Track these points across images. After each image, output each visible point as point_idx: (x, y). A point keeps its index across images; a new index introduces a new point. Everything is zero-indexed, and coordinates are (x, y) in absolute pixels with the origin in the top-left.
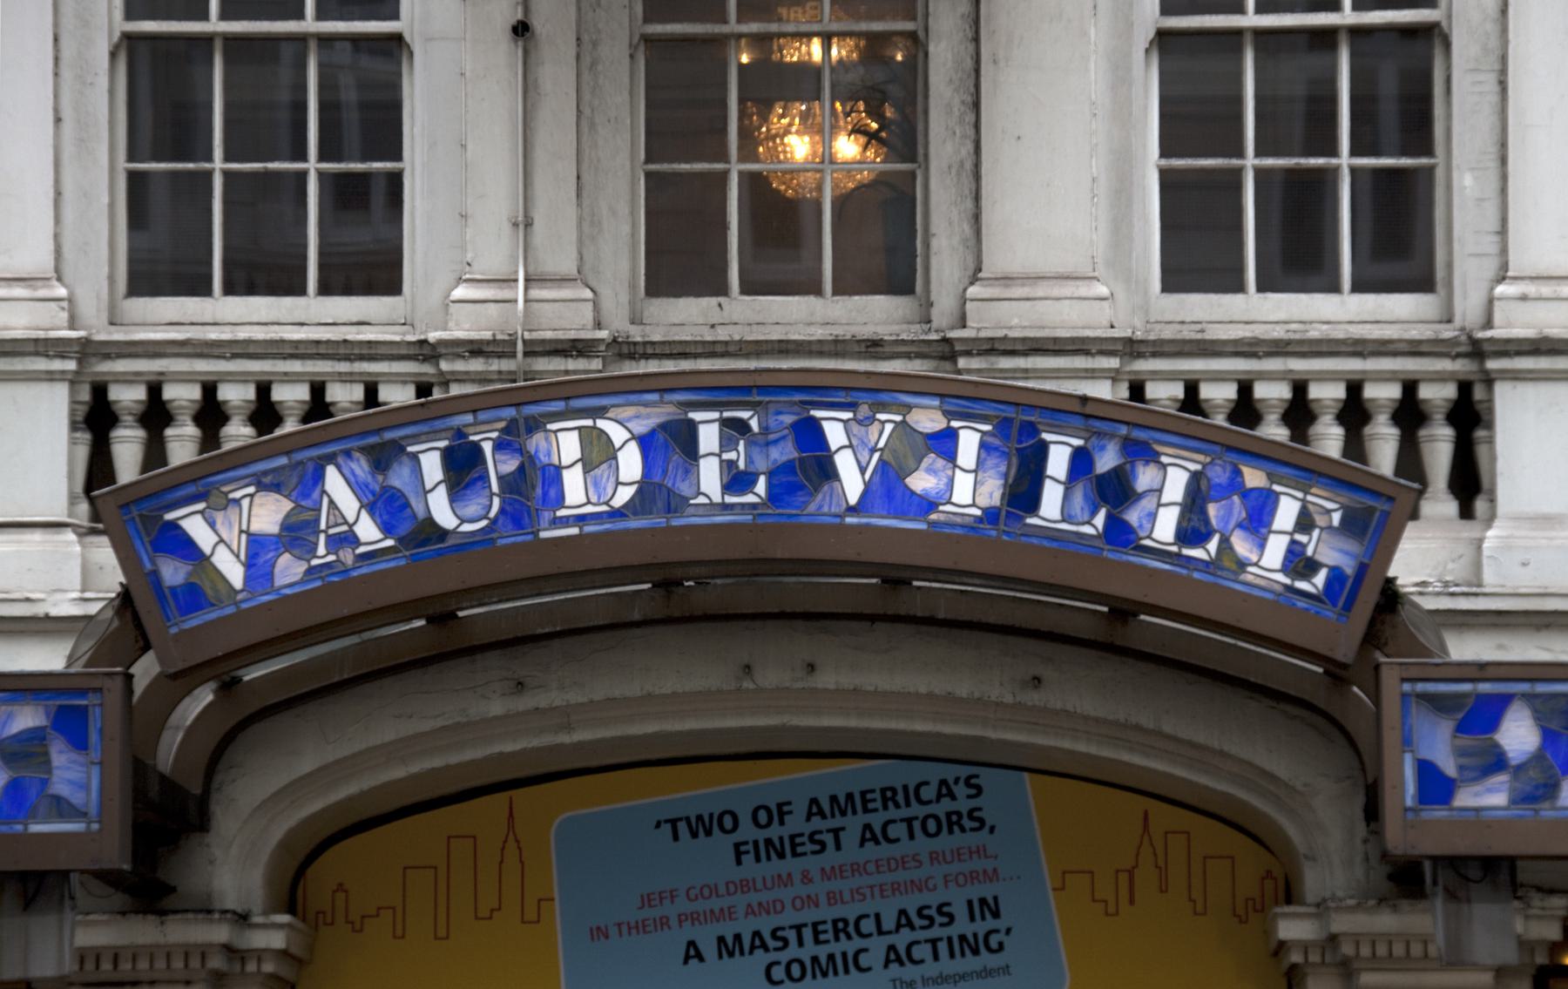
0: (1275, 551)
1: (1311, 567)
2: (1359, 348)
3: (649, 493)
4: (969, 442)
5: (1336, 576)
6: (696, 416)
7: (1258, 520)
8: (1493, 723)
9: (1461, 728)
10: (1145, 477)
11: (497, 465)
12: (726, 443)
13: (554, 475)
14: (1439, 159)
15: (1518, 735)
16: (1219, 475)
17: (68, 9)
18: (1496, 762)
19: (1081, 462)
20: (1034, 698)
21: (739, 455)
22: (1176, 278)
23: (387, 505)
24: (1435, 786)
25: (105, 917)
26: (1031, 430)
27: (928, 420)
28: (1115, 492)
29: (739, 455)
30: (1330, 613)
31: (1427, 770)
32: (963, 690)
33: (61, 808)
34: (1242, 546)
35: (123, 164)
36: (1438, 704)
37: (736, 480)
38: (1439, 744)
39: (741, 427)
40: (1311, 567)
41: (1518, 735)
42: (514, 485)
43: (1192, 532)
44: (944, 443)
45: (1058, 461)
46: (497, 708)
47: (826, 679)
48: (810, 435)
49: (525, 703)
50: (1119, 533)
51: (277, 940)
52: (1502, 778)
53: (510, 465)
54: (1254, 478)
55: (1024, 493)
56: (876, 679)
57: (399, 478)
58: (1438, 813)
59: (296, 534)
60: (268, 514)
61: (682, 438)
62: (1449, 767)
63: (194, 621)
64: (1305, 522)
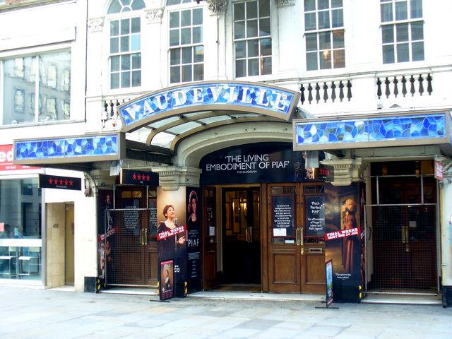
0: (277, 103)
1: (282, 106)
2: (341, 76)
3: (188, 102)
4: (232, 89)
5: (286, 107)
6: (194, 89)
7: (274, 98)
8: (309, 129)
9: (305, 130)
10: (258, 94)
11: (167, 99)
12: (198, 93)
13: (174, 100)
14: (169, 29)
15: (313, 131)
16: (269, 92)
17: (450, 68)
18: (310, 135)
19: (248, 91)
20: (286, 132)
21: (200, 95)
22: (309, 68)
23: (153, 106)
24: (301, 140)
25: (14, 167)
26: (241, 87)
27: (226, 87)
28: (253, 96)
29: (200, 95)
30: (285, 113)
31: (300, 137)
32: (276, 131)
33: (113, 152)
34: (272, 103)
35: (170, 66)
36: (302, 126)
37: (200, 99)
38: (302, 133)
39: (200, 90)
40: (282, 106)
41: (313, 131)
42: (169, 102)
43: (265, 102)
44: (228, 90)
45: (245, 93)
46: (213, 137)
47: (256, 131)
48: (209, 91)
49: (217, 136)
50: (254, 103)
51: (186, 170)
52: (311, 138)
53: (169, 99)
54: (274, 92)
55: (240, 98)
56: (269, 130)
57: (154, 102)
58: (301, 144)
59: (142, 111)
60: (138, 108)
61: (192, 93)
62: (303, 136)
63: (130, 123)
64: (281, 99)
